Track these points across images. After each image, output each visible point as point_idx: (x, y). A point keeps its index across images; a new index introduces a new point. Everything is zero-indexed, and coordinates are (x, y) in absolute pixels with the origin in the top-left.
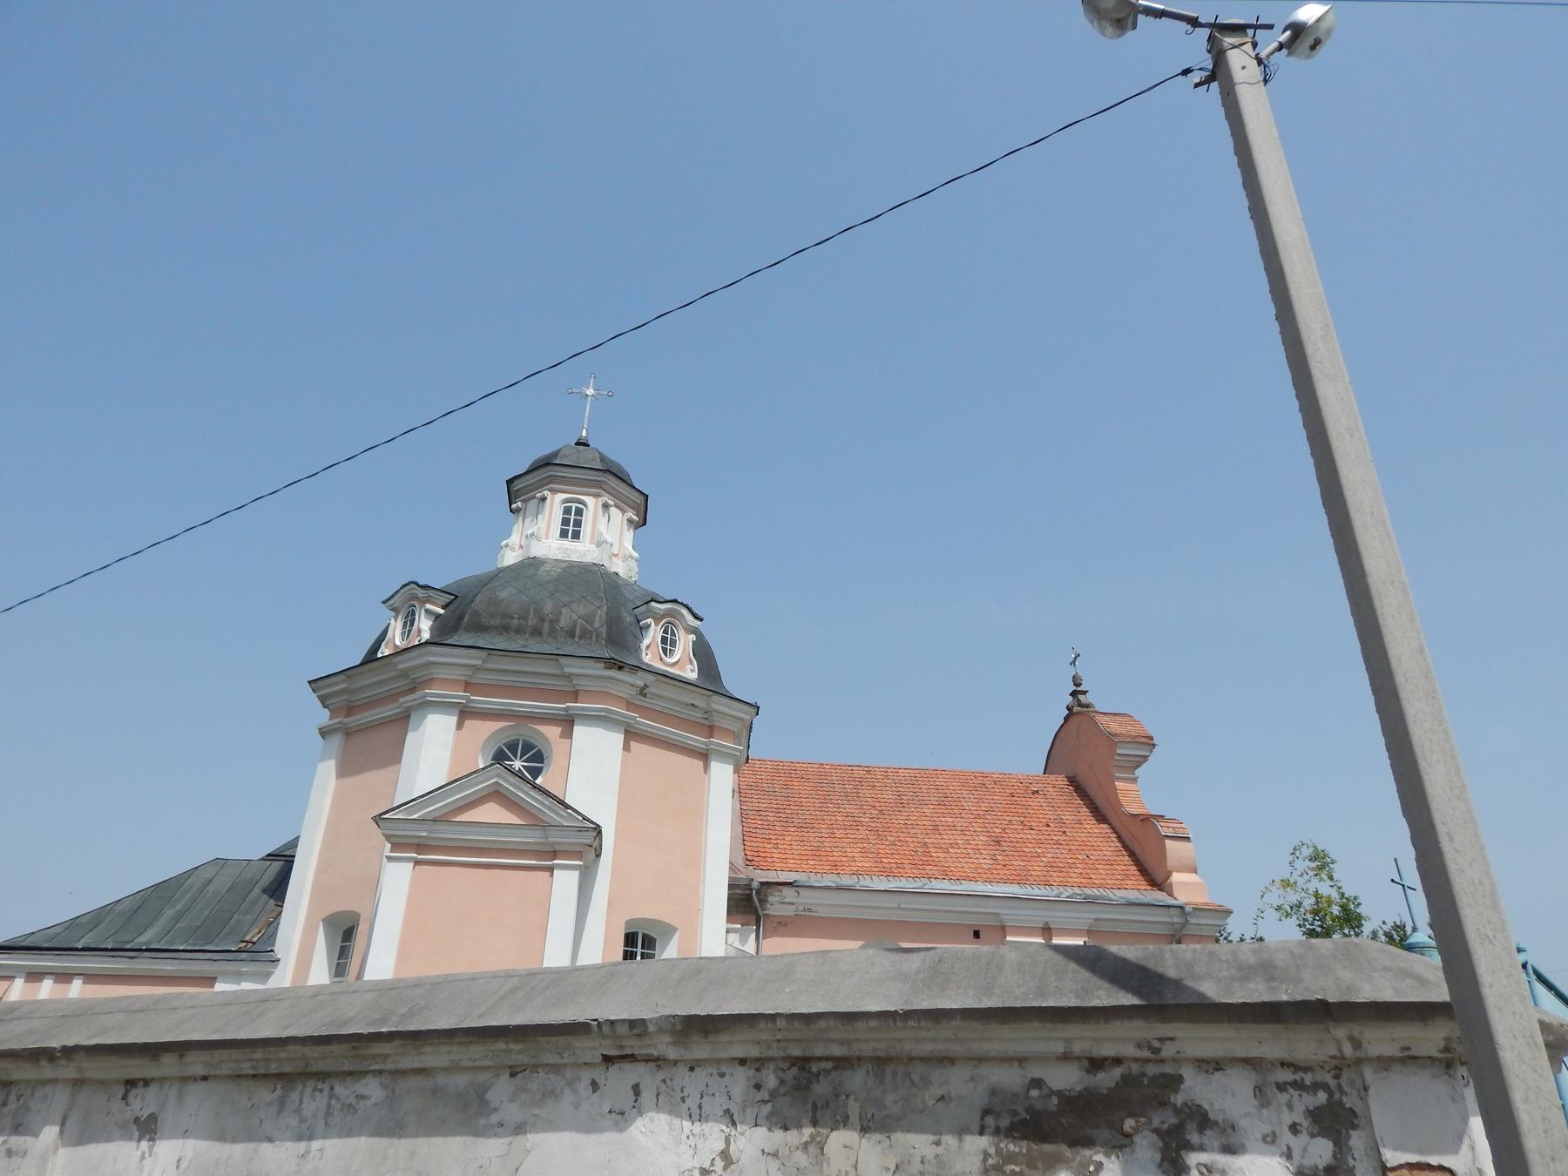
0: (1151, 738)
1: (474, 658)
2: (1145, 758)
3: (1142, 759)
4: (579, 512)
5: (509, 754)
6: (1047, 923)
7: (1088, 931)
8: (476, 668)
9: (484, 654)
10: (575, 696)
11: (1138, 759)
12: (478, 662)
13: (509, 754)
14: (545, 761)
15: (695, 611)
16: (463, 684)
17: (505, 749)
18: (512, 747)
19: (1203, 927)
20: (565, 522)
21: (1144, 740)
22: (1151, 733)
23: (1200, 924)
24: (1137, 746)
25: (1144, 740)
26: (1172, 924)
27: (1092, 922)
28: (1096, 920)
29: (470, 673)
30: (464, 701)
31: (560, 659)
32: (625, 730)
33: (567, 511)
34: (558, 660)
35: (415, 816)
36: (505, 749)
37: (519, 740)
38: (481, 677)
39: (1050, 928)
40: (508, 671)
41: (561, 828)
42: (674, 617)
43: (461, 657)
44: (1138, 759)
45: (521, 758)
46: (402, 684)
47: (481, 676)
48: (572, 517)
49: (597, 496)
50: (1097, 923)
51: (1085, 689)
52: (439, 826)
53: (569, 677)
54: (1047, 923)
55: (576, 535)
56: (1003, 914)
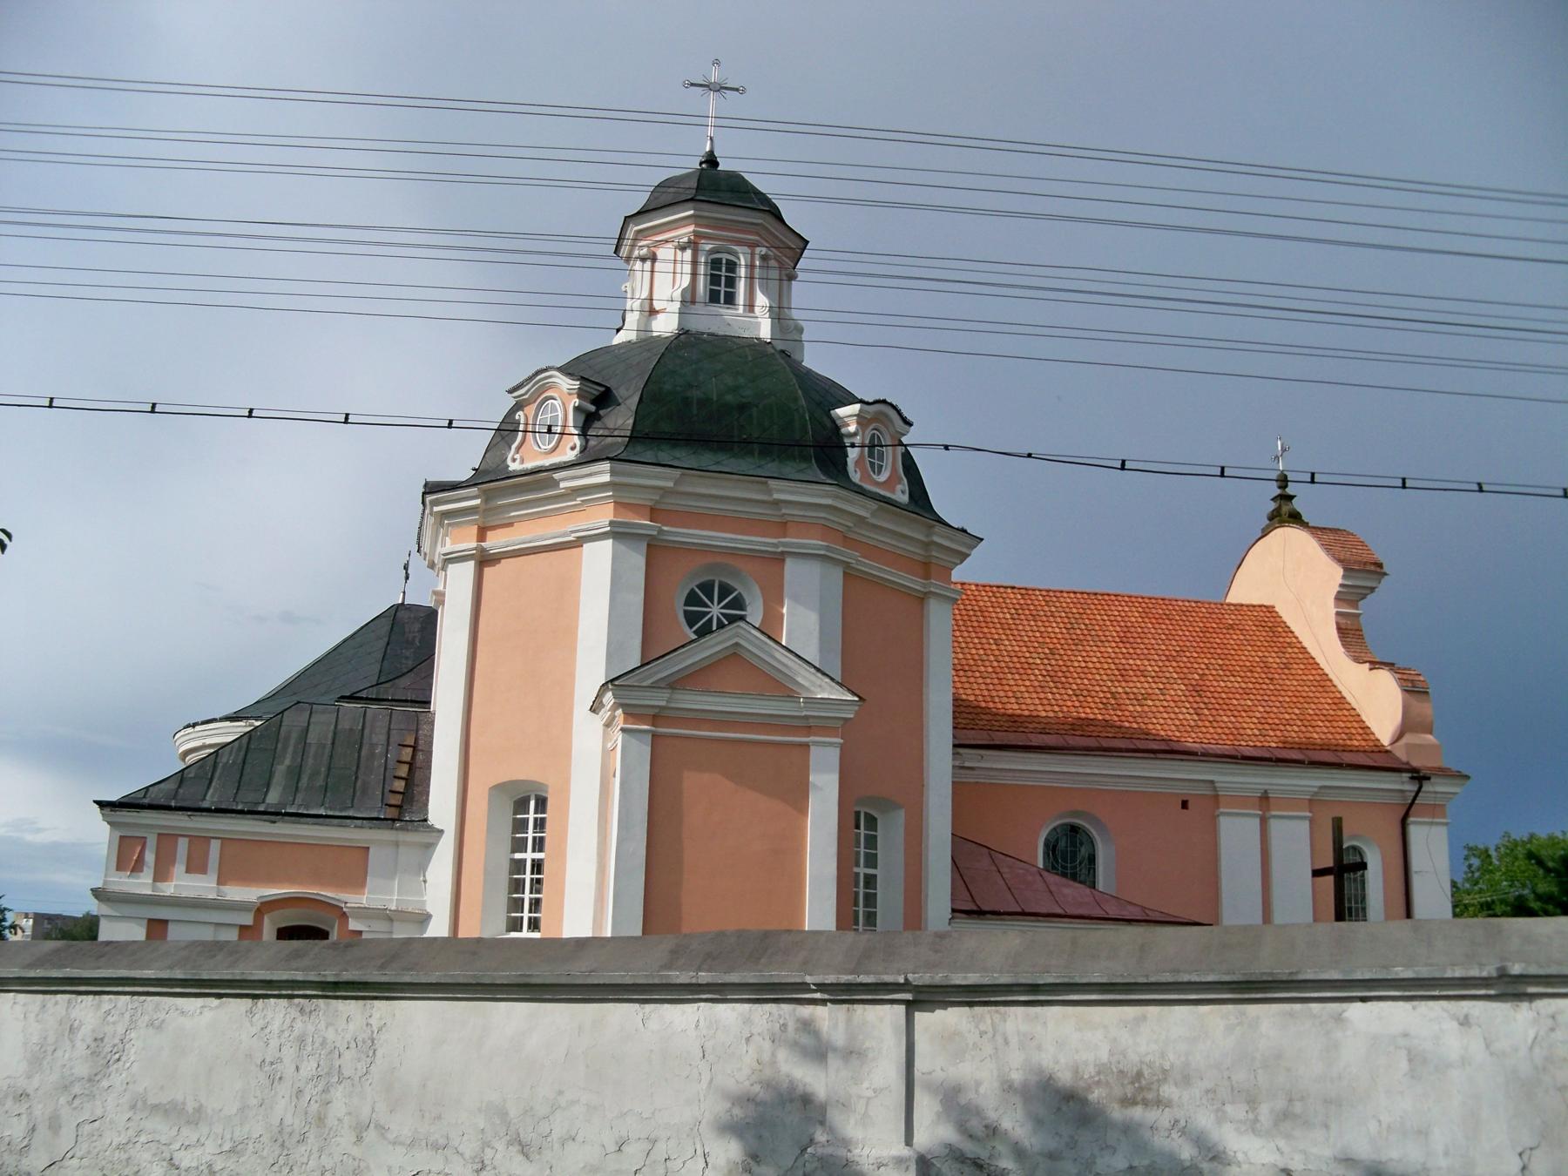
0: (1380, 565)
1: (665, 479)
2: (1372, 589)
3: (1368, 592)
4: (732, 266)
5: (704, 598)
6: (1266, 791)
7: (1310, 800)
8: (665, 492)
9: (874, 505)
10: (783, 527)
11: (1359, 591)
12: (670, 484)
13: (704, 598)
14: (748, 608)
15: (905, 414)
16: (649, 509)
17: (734, 595)
18: (707, 588)
19: (1439, 795)
20: (715, 280)
21: (1373, 568)
22: (1381, 559)
23: (1436, 793)
24: (1364, 575)
25: (1373, 568)
26: (1402, 791)
27: (1316, 790)
28: (1321, 787)
29: (658, 498)
30: (655, 533)
31: (771, 482)
32: (648, 545)
33: (715, 264)
34: (766, 483)
35: (644, 684)
36: (734, 595)
37: (736, 590)
38: (673, 503)
39: (1218, 795)
40: (728, 498)
41: (829, 702)
42: (882, 423)
43: (656, 477)
44: (1359, 591)
45: (707, 606)
46: (917, 551)
47: (673, 501)
48: (723, 273)
49: (753, 245)
50: (1323, 791)
51: (1292, 493)
52: (679, 695)
53: (777, 504)
54: (1266, 791)
55: (730, 299)
56: (1218, 782)
